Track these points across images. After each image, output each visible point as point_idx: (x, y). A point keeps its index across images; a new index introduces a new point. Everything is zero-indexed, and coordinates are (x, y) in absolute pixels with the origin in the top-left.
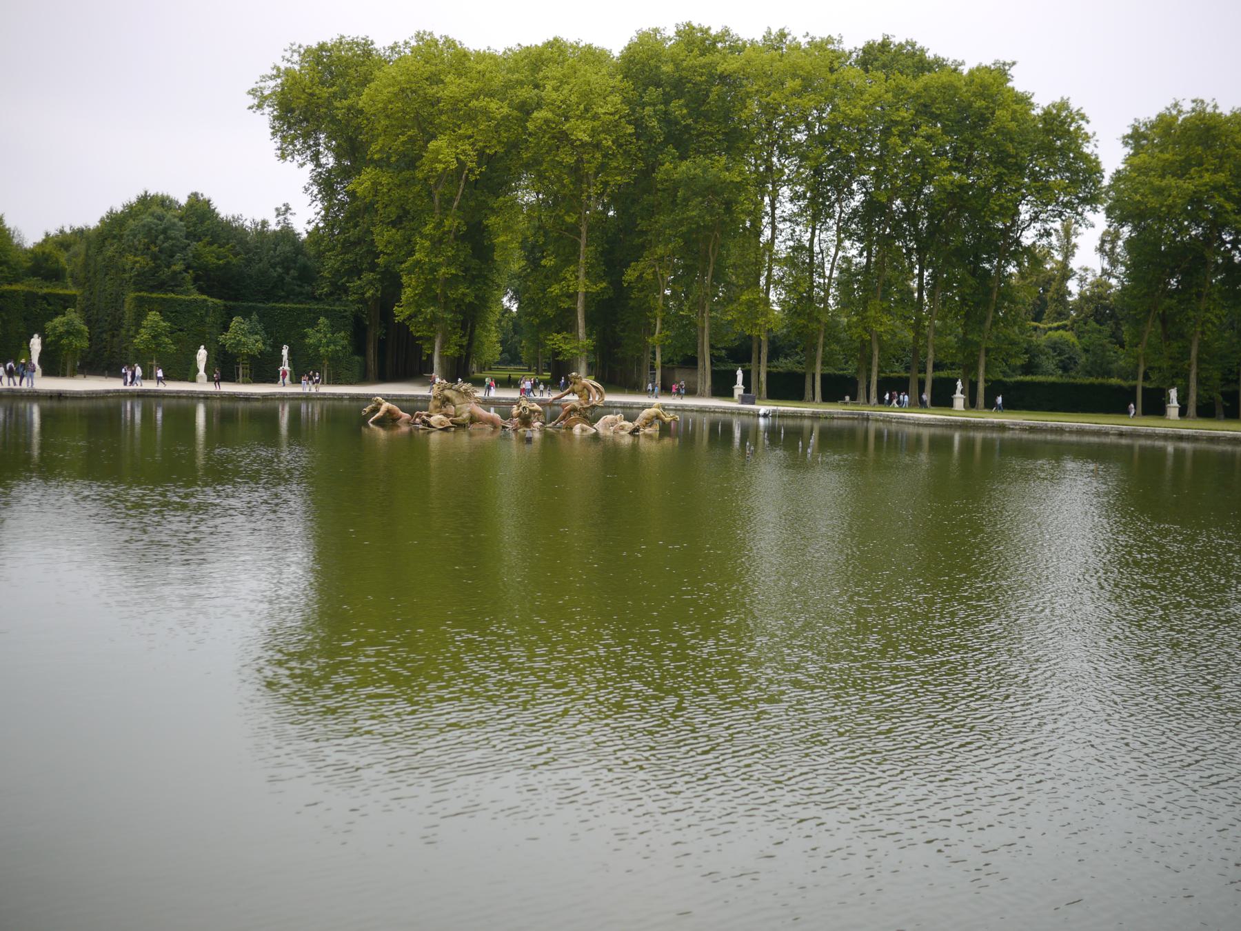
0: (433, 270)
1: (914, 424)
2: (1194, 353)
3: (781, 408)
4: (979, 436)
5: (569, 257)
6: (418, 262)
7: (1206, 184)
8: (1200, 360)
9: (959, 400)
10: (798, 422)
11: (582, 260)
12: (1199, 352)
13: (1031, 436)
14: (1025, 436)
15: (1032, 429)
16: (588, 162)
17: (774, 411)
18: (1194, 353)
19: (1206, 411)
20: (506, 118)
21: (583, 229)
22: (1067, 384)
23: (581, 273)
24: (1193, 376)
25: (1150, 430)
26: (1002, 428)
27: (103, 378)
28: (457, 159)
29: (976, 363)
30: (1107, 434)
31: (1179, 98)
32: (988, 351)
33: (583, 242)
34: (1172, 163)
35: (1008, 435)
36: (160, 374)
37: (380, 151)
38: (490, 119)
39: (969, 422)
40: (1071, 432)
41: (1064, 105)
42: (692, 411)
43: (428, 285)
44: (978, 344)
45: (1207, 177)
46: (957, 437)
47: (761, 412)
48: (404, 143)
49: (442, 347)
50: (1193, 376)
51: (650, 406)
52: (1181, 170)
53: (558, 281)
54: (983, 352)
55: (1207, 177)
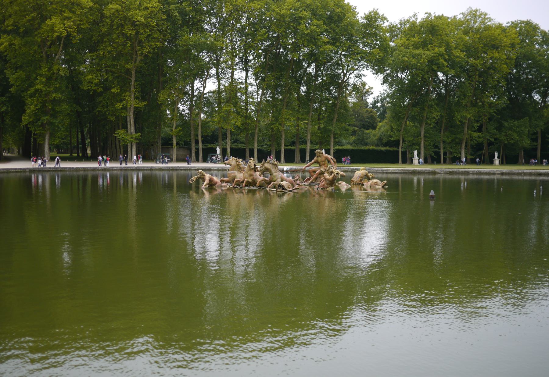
0: (47, 94)
1: (381, 173)
2: (422, 133)
3: (294, 167)
4: (422, 178)
5: (125, 86)
6: (37, 91)
7: (436, 53)
8: (425, 137)
9: (497, 161)
10: (492, 177)
11: (133, 89)
12: (425, 133)
13: (450, 177)
14: (448, 176)
15: (451, 173)
16: (142, 34)
17: (291, 169)
18: (422, 133)
19: (426, 162)
20: (91, 8)
21: (133, 72)
22: (358, 150)
23: (132, 97)
24: (422, 145)
25: (520, 171)
26: (434, 173)
27: (88, 162)
28: (67, 30)
29: (330, 141)
30: (494, 174)
31: (416, 12)
32: (335, 134)
33: (133, 79)
34: (419, 42)
35: (437, 176)
36: (524, 161)
37: (12, 25)
38: (82, 8)
39: (416, 170)
40: (473, 173)
41: (376, 13)
42: (147, 170)
43: (44, 105)
44: (330, 131)
45: (437, 49)
46: (415, 179)
47: (285, 169)
48: (29, 21)
49: (49, 139)
50: (422, 145)
52: (424, 45)
53: (121, 101)
54: (332, 136)
55: (437, 49)
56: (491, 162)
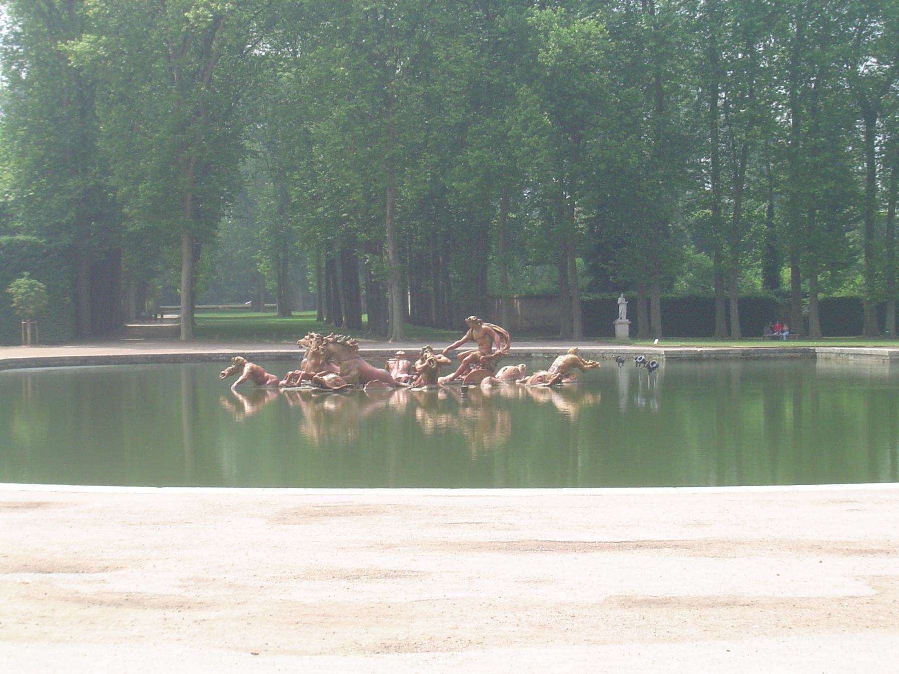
51: (564, 353)
56: (607, 333)
